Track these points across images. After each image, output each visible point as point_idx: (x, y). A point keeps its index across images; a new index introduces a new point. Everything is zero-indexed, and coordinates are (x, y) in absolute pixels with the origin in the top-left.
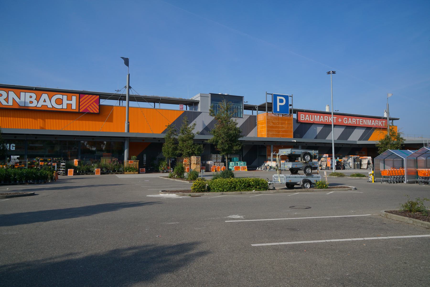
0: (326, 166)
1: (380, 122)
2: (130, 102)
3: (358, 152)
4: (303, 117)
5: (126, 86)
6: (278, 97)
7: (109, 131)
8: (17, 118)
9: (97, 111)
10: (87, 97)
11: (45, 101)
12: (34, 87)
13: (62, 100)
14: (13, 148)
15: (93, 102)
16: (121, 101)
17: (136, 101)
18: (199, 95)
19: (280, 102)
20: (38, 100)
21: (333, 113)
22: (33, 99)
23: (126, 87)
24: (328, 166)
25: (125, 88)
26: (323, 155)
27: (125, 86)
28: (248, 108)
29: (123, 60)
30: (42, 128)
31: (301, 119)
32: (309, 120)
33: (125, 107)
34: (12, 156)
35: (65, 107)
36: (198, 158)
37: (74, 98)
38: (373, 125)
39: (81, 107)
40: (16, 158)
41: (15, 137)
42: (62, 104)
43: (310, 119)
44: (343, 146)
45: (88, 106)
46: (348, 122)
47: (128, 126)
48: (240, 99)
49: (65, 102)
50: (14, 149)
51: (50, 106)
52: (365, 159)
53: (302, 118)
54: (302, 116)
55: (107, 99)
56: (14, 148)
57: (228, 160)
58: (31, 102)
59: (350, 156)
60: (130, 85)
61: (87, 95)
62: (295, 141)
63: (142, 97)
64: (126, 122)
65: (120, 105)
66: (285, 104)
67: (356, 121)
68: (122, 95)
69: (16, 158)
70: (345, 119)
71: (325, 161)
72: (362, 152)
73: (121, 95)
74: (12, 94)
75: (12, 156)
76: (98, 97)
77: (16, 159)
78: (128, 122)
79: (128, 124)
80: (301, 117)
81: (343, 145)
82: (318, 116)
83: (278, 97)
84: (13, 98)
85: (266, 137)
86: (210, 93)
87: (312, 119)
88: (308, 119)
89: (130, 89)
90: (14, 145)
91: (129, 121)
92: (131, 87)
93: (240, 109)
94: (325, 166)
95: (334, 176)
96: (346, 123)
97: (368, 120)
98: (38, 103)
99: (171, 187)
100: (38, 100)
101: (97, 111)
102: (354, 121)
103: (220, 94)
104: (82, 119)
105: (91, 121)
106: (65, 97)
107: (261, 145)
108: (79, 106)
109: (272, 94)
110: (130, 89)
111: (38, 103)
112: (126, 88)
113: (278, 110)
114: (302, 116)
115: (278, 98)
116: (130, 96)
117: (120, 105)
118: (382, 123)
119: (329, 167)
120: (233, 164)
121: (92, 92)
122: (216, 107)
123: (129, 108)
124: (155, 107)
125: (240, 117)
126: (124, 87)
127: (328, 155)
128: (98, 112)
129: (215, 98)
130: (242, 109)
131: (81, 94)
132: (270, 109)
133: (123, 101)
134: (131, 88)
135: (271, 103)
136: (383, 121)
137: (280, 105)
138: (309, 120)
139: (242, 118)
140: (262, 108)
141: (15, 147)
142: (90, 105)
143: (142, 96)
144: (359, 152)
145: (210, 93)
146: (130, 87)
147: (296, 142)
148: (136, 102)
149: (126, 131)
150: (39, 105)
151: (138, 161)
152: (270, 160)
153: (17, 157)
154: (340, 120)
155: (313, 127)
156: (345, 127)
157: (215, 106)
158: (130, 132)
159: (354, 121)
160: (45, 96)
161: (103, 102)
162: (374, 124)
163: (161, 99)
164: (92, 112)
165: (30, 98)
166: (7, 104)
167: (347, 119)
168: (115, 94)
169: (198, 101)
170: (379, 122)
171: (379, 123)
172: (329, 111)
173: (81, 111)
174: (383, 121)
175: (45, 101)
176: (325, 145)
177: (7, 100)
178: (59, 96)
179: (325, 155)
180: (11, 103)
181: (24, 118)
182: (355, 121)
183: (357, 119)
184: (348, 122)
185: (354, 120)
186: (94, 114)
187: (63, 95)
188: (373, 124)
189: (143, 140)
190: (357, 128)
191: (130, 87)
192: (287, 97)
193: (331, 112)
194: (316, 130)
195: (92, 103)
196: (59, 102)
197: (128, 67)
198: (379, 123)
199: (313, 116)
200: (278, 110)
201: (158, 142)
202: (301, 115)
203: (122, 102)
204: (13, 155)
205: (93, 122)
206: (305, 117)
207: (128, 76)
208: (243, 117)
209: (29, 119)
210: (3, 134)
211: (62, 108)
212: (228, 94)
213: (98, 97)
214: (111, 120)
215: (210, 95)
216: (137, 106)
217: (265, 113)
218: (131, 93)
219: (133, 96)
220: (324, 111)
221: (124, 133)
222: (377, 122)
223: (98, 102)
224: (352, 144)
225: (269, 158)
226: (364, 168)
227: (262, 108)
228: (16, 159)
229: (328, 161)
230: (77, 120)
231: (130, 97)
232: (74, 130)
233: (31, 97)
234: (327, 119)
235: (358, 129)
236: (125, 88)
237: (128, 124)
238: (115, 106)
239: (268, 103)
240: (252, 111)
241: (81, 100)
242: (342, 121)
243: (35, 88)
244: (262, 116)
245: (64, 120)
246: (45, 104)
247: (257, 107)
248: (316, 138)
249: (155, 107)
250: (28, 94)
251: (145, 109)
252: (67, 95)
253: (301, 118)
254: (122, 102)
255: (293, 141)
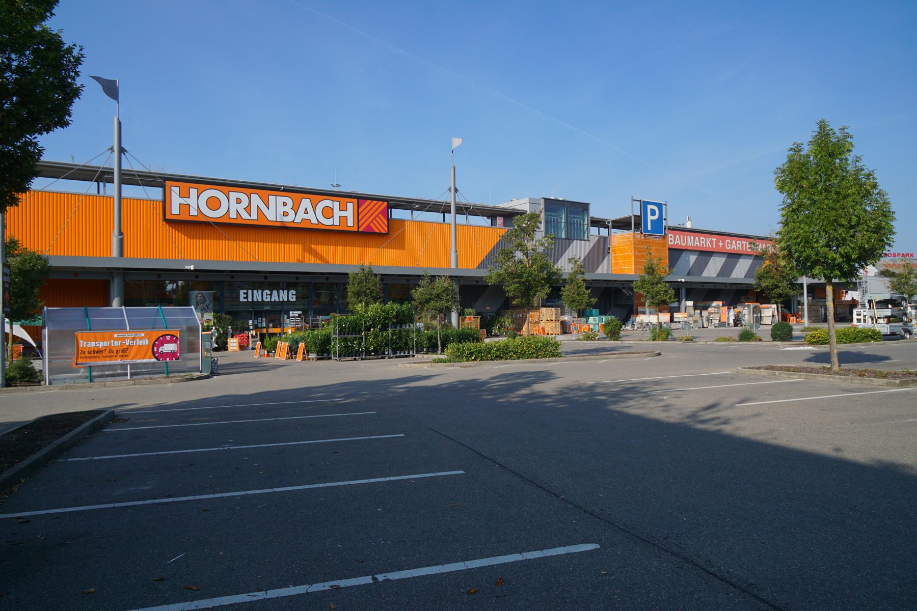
0: (720, 321)
1: (708, 239)
2: (122, 185)
3: (744, 297)
4: (672, 239)
5: (113, 146)
6: (648, 206)
7: (212, 259)
8: (329, 247)
9: (385, 230)
10: (381, 205)
11: (306, 212)
12: (281, 186)
13: (333, 209)
14: (267, 298)
15: (379, 214)
16: (101, 184)
17: (141, 185)
18: (527, 200)
19: (651, 215)
20: (296, 209)
21: (456, 204)
22: (288, 209)
23: (112, 149)
24: (722, 321)
25: (111, 153)
26: (712, 303)
27: (110, 146)
28: (597, 223)
29: (100, 85)
30: (300, 261)
31: (670, 243)
32: (680, 244)
33: (112, 198)
34: (291, 312)
35: (337, 223)
36: (556, 311)
37: (350, 206)
38: (734, 248)
39: (361, 223)
40: (297, 315)
41: (607, 284)
42: (333, 217)
43: (680, 242)
44: (715, 286)
45: (372, 222)
46: (731, 247)
47: (121, 242)
48: (584, 208)
49: (337, 213)
50: (294, 300)
51: (314, 221)
52: (768, 308)
53: (671, 241)
54: (671, 237)
55: (62, 178)
56: (294, 297)
57: (781, 309)
58: (286, 214)
59: (746, 304)
60: (122, 146)
61: (369, 201)
62: (683, 280)
63: (156, 175)
64: (116, 232)
65: (99, 192)
66: (657, 219)
67: (742, 244)
68: (103, 168)
69: (297, 315)
70: (728, 242)
71: (717, 313)
72: (749, 298)
73: (100, 170)
74: (256, 199)
75: (291, 312)
76: (386, 203)
77: (297, 317)
78: (121, 233)
79: (121, 237)
80: (670, 239)
81: (408, 277)
82: (692, 237)
83: (648, 206)
84: (268, 209)
85: (633, 274)
86: (543, 198)
87: (684, 243)
88: (679, 242)
89: (124, 154)
90: (294, 292)
91: (122, 231)
92: (126, 148)
93: (584, 225)
94: (718, 320)
95: (808, 331)
96: (728, 248)
97: (688, 237)
98: (296, 215)
99: (742, 345)
100: (296, 209)
101: (385, 230)
102: (671, 239)
103: (552, 198)
104: (361, 244)
105: (333, 246)
106: (336, 204)
107: (615, 287)
108: (358, 221)
109: (640, 201)
110: (124, 154)
111: (296, 215)
112: (114, 151)
113: (649, 228)
114: (671, 237)
115: (650, 207)
116: (123, 172)
117: (99, 192)
118: (711, 242)
119: (725, 322)
120: (597, 319)
121: (200, 178)
122: (551, 222)
123: (122, 200)
124: (600, 233)
125: (581, 240)
126: (109, 150)
127: (721, 302)
128: (387, 231)
129: (552, 205)
130: (588, 225)
131: (360, 199)
132: (638, 225)
133: (107, 184)
134: (126, 151)
135: (638, 216)
136: (713, 239)
137: (651, 220)
138: (680, 244)
139: (588, 240)
140: (622, 224)
141: (295, 296)
142: (375, 219)
143: (154, 173)
144: (745, 298)
145: (544, 197)
146: (122, 151)
147: (685, 282)
148: (141, 187)
149: (115, 253)
150: (298, 220)
151: (479, 317)
152: (644, 313)
153: (299, 314)
154: (721, 244)
155: (684, 255)
156: (698, 253)
157: (549, 220)
158: (125, 256)
159: (671, 239)
160: (306, 203)
161: (397, 214)
162: (735, 247)
163: (473, 208)
164: (377, 231)
165: (284, 206)
166: (249, 218)
167: (730, 242)
168: (83, 166)
169: (525, 211)
170: (706, 240)
171: (706, 242)
172: (692, 226)
173: (361, 230)
174: (713, 239)
175: (306, 212)
176: (703, 286)
177: (248, 209)
178: (327, 203)
179: (715, 304)
180: (254, 216)
181: (194, 239)
182: (740, 246)
183: (743, 242)
184: (731, 247)
185: (739, 244)
186: (380, 234)
187: (333, 201)
188: (696, 243)
189: (76, 274)
190: (742, 257)
191: (122, 151)
192: (659, 206)
193: (113, 169)
194: (688, 261)
195: (377, 216)
196: (328, 213)
197: (116, 102)
198: (706, 242)
199: (682, 236)
200: (649, 228)
201: (475, 283)
202: (670, 235)
203: (104, 186)
204: (292, 311)
205: (329, 247)
206: (674, 239)
207: (452, 170)
208: (590, 240)
209: (322, 246)
210: (285, 274)
211: (333, 225)
212: (565, 198)
213: (386, 203)
214: (401, 246)
215: (542, 201)
216: (144, 196)
217: (629, 234)
218: (457, 200)
219: (461, 205)
220: (410, 198)
221: (111, 258)
222: (703, 240)
223: (386, 213)
224: (461, 277)
225: (640, 309)
226: (766, 323)
227: (622, 224)
228: (297, 317)
229: (723, 312)
230: (383, 248)
231: (124, 174)
232: (283, 261)
233: (285, 204)
234: (704, 242)
235: (745, 259)
236: (110, 151)
237: (121, 237)
238: (86, 196)
239: (635, 216)
240: (597, 228)
241: (361, 210)
242: (724, 246)
243: (284, 187)
244: (619, 237)
245: (204, 240)
246: (306, 216)
247: (610, 223)
248: (689, 274)
249: (444, 221)
250: (281, 200)
251: (62, 195)
252: (179, 187)
253: (669, 241)
254: (104, 186)
255: (679, 280)
